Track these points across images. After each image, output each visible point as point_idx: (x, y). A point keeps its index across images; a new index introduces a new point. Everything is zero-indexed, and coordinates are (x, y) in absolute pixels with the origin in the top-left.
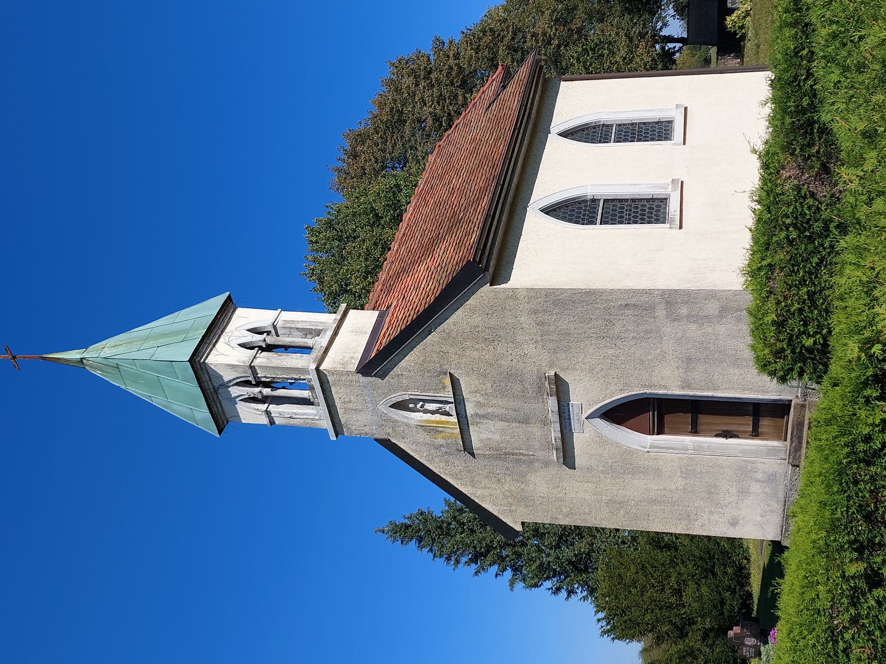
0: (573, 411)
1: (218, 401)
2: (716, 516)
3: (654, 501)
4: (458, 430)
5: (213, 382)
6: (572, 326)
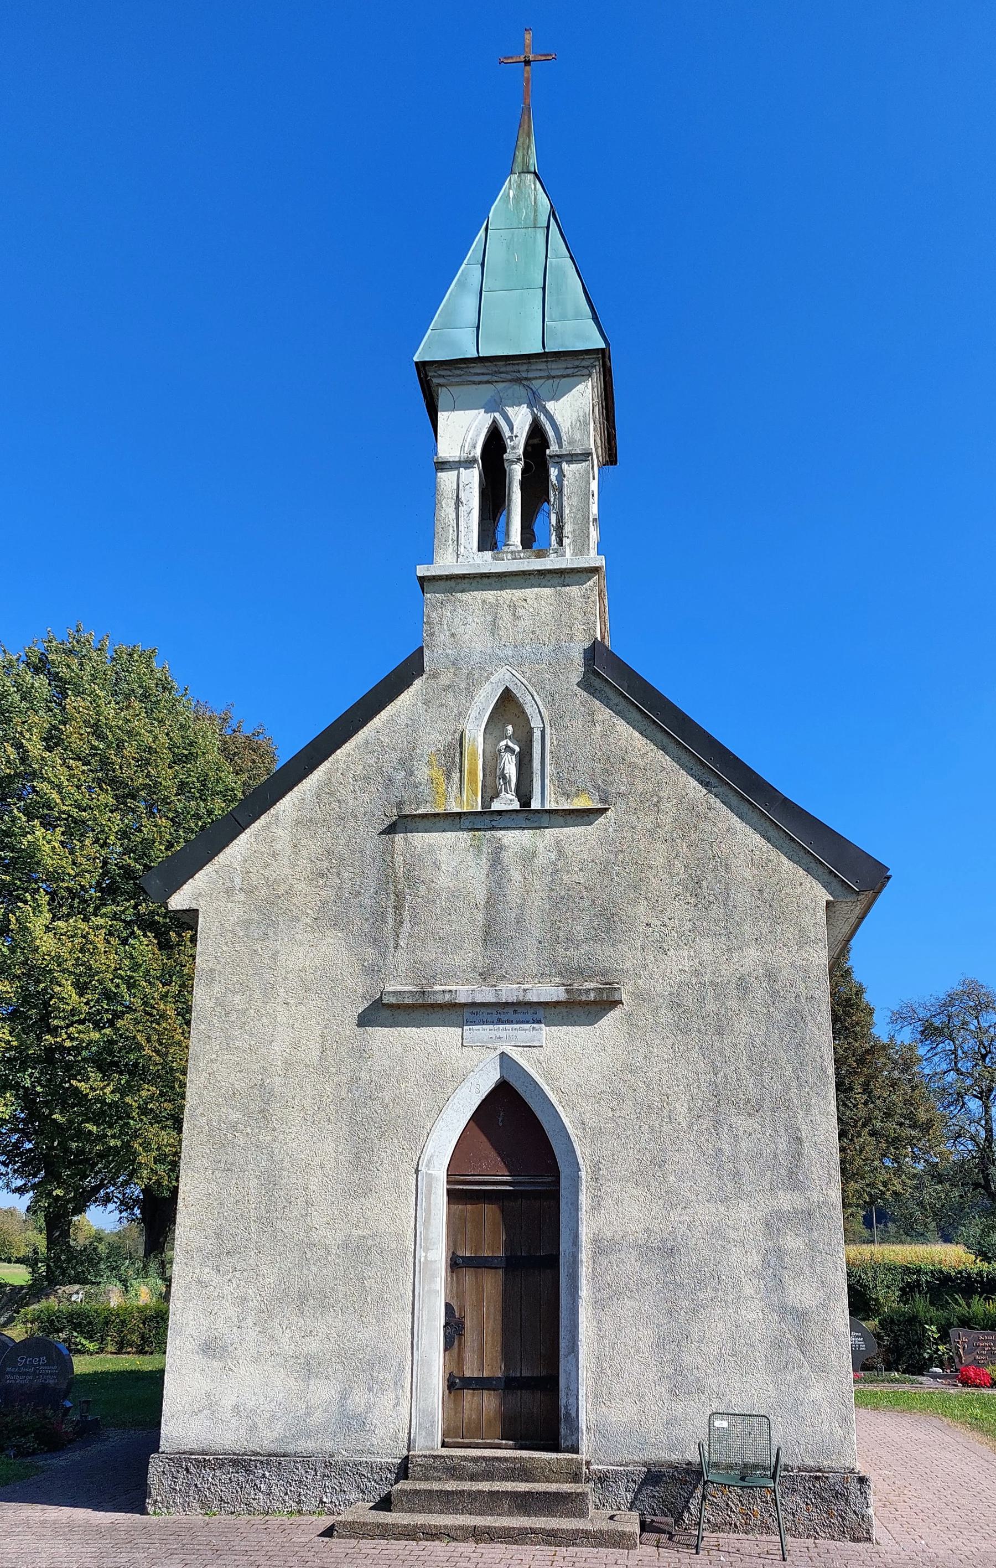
0: (506, 1029)
1: (495, 378)
2: (231, 1312)
3: (270, 1181)
4: (457, 810)
5: (543, 381)
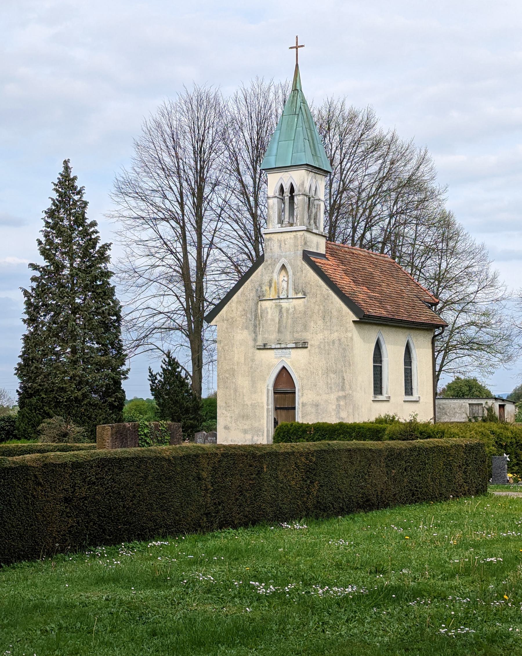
2: (229, 420)
3: (236, 390)
6: (333, 356)
